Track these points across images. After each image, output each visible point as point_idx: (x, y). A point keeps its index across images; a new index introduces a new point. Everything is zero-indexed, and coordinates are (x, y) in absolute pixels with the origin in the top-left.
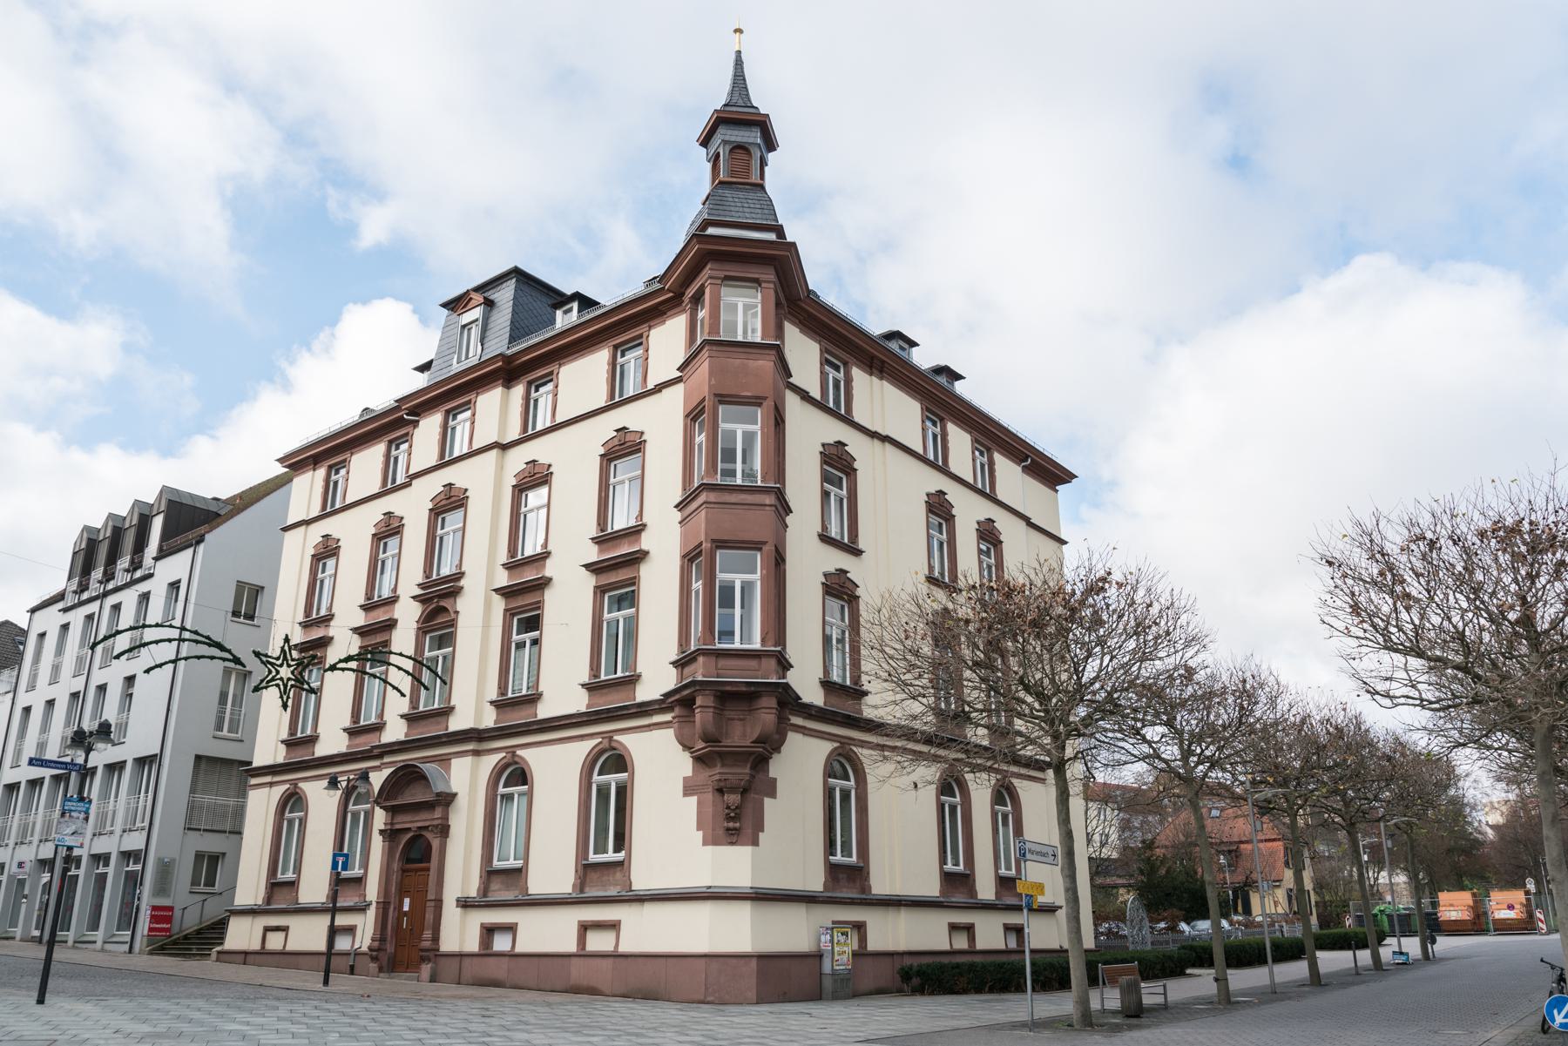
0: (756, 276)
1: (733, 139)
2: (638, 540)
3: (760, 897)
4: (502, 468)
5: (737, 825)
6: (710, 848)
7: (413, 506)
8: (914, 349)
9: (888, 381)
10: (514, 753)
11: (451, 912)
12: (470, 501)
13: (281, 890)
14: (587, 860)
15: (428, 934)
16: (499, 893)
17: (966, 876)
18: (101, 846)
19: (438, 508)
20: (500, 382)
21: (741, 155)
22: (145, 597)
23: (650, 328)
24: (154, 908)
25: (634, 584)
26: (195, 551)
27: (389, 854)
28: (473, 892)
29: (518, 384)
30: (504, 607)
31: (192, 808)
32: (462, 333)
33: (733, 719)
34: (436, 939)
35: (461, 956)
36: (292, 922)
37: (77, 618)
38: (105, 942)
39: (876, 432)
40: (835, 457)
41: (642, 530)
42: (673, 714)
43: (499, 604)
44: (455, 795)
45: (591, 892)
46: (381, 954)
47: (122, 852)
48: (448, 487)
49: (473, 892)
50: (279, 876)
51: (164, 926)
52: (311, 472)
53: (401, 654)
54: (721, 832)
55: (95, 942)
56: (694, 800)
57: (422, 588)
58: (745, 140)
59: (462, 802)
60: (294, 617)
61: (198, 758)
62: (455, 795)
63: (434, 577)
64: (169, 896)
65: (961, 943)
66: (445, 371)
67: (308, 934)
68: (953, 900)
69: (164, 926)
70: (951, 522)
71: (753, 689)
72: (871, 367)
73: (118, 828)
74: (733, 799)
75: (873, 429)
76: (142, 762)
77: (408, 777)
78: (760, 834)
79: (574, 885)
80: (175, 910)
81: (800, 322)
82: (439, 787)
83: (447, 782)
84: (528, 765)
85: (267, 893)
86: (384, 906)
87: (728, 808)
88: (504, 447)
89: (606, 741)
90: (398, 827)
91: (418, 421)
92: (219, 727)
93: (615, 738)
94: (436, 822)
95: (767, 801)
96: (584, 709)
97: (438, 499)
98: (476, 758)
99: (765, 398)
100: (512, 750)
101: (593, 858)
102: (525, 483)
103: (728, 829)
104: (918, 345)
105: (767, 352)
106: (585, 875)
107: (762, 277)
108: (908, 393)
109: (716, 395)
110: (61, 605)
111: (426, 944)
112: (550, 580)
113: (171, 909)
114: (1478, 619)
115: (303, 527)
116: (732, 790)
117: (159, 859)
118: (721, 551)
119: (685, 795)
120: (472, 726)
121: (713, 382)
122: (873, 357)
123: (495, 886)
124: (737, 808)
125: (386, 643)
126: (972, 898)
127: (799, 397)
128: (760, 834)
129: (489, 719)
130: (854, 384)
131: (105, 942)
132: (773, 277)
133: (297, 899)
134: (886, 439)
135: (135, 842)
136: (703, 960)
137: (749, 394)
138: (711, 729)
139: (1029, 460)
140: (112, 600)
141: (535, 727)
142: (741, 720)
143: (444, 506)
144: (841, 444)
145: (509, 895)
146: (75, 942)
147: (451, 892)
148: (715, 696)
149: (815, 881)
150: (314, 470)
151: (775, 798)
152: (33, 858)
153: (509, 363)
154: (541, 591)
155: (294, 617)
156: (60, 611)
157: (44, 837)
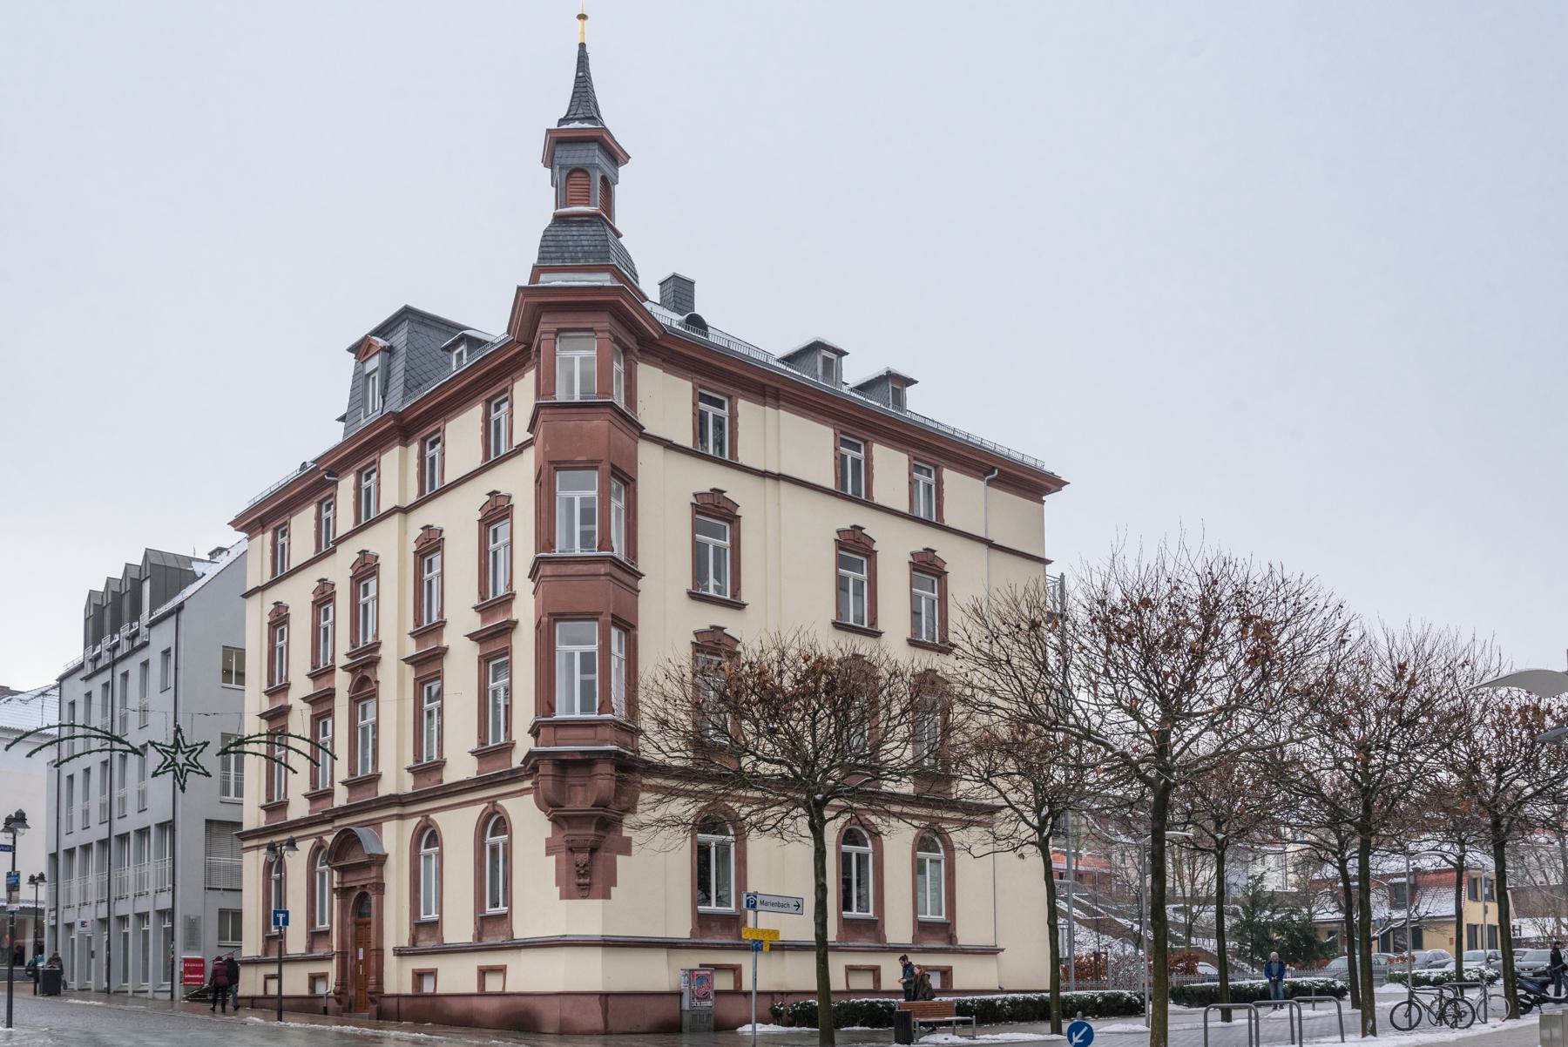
0: (589, 326)
1: (569, 161)
2: (509, 610)
3: (609, 944)
4: (406, 533)
5: (587, 881)
6: (565, 901)
7: (338, 570)
8: (844, 358)
9: (786, 409)
10: (494, 803)
11: (390, 961)
12: (446, 542)
13: (275, 941)
14: (484, 912)
15: (372, 979)
16: (426, 943)
17: (876, 921)
18: (144, 905)
19: (357, 576)
20: (397, 440)
21: (578, 179)
22: (145, 664)
23: (513, 381)
24: (186, 961)
25: (506, 654)
26: (177, 620)
27: (343, 908)
28: (405, 943)
29: (347, 475)
30: (478, 653)
31: (209, 869)
32: (367, 383)
33: (574, 786)
34: (380, 983)
35: (398, 996)
36: (744, 961)
37: (96, 685)
38: (155, 992)
39: (766, 472)
40: (711, 507)
41: (513, 599)
42: (531, 781)
43: (410, 673)
44: (386, 856)
45: (488, 941)
46: (343, 996)
47: (158, 911)
48: (426, 530)
49: (405, 943)
50: (318, 926)
51: (198, 976)
52: (261, 536)
53: (299, 737)
54: (573, 887)
55: (147, 992)
56: (553, 858)
57: (352, 658)
58: (582, 161)
59: (391, 863)
60: (261, 686)
61: (209, 823)
62: (386, 856)
63: (361, 645)
64: (199, 949)
65: (865, 982)
66: (355, 426)
67: (295, 982)
68: (850, 944)
69: (198, 976)
70: (873, 559)
71: (587, 757)
72: (764, 396)
73: (151, 890)
74: (583, 857)
75: (762, 468)
76: (162, 826)
77: (348, 840)
78: (613, 888)
79: (474, 936)
80: (206, 962)
81: (664, 360)
82: (374, 850)
83: (379, 842)
84: (507, 814)
85: (264, 946)
86: (343, 955)
87: (577, 866)
88: (405, 511)
89: (491, 805)
90: (348, 885)
91: (337, 482)
92: (226, 792)
93: (499, 802)
94: (372, 881)
95: (620, 859)
96: (474, 775)
97: (356, 567)
98: (400, 822)
99: (600, 461)
100: (425, 814)
101: (489, 911)
102: (425, 549)
103: (579, 885)
104: (847, 354)
105: (602, 410)
106: (482, 926)
107: (596, 326)
108: (814, 419)
109: (551, 462)
110: (82, 674)
111: (372, 988)
112: (516, 623)
113: (201, 961)
114: (1116, 692)
115: (259, 595)
116: (581, 849)
117: (185, 917)
118: (562, 623)
119: (548, 854)
120: (394, 792)
121: (548, 449)
122: (764, 386)
123: (422, 937)
124: (585, 865)
125: (285, 727)
126: (879, 942)
127: (662, 448)
128: (613, 888)
129: (408, 785)
130: (739, 420)
131: (155, 992)
132: (607, 324)
133: (443, 939)
134: (779, 477)
135: (164, 902)
136: (557, 998)
137: (584, 458)
138: (551, 795)
139: (996, 471)
140: (120, 669)
141: (440, 793)
142: (581, 786)
143: (363, 573)
144: (717, 492)
145: (500, 940)
146: (134, 992)
147: (389, 944)
148: (554, 765)
149: (682, 928)
150: (263, 533)
151: (630, 855)
152: (94, 918)
153: (402, 420)
154: (439, 661)
155: (261, 686)
156: (82, 680)
157: (118, 895)
